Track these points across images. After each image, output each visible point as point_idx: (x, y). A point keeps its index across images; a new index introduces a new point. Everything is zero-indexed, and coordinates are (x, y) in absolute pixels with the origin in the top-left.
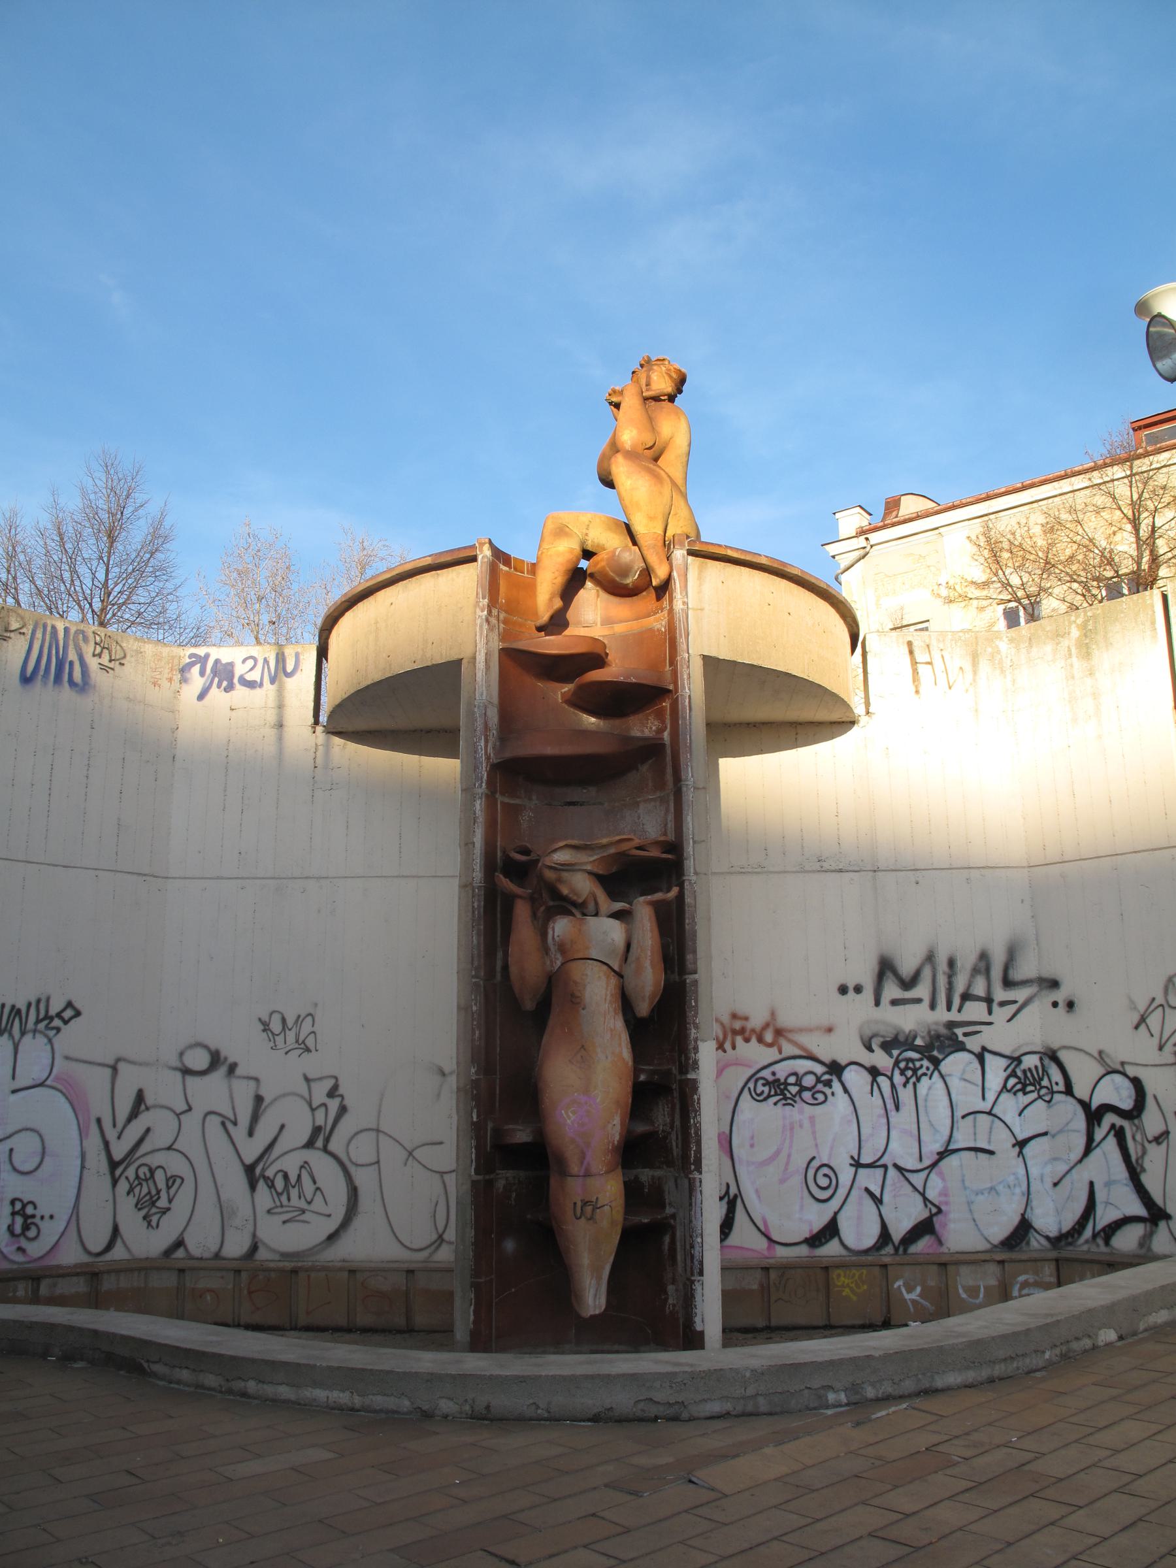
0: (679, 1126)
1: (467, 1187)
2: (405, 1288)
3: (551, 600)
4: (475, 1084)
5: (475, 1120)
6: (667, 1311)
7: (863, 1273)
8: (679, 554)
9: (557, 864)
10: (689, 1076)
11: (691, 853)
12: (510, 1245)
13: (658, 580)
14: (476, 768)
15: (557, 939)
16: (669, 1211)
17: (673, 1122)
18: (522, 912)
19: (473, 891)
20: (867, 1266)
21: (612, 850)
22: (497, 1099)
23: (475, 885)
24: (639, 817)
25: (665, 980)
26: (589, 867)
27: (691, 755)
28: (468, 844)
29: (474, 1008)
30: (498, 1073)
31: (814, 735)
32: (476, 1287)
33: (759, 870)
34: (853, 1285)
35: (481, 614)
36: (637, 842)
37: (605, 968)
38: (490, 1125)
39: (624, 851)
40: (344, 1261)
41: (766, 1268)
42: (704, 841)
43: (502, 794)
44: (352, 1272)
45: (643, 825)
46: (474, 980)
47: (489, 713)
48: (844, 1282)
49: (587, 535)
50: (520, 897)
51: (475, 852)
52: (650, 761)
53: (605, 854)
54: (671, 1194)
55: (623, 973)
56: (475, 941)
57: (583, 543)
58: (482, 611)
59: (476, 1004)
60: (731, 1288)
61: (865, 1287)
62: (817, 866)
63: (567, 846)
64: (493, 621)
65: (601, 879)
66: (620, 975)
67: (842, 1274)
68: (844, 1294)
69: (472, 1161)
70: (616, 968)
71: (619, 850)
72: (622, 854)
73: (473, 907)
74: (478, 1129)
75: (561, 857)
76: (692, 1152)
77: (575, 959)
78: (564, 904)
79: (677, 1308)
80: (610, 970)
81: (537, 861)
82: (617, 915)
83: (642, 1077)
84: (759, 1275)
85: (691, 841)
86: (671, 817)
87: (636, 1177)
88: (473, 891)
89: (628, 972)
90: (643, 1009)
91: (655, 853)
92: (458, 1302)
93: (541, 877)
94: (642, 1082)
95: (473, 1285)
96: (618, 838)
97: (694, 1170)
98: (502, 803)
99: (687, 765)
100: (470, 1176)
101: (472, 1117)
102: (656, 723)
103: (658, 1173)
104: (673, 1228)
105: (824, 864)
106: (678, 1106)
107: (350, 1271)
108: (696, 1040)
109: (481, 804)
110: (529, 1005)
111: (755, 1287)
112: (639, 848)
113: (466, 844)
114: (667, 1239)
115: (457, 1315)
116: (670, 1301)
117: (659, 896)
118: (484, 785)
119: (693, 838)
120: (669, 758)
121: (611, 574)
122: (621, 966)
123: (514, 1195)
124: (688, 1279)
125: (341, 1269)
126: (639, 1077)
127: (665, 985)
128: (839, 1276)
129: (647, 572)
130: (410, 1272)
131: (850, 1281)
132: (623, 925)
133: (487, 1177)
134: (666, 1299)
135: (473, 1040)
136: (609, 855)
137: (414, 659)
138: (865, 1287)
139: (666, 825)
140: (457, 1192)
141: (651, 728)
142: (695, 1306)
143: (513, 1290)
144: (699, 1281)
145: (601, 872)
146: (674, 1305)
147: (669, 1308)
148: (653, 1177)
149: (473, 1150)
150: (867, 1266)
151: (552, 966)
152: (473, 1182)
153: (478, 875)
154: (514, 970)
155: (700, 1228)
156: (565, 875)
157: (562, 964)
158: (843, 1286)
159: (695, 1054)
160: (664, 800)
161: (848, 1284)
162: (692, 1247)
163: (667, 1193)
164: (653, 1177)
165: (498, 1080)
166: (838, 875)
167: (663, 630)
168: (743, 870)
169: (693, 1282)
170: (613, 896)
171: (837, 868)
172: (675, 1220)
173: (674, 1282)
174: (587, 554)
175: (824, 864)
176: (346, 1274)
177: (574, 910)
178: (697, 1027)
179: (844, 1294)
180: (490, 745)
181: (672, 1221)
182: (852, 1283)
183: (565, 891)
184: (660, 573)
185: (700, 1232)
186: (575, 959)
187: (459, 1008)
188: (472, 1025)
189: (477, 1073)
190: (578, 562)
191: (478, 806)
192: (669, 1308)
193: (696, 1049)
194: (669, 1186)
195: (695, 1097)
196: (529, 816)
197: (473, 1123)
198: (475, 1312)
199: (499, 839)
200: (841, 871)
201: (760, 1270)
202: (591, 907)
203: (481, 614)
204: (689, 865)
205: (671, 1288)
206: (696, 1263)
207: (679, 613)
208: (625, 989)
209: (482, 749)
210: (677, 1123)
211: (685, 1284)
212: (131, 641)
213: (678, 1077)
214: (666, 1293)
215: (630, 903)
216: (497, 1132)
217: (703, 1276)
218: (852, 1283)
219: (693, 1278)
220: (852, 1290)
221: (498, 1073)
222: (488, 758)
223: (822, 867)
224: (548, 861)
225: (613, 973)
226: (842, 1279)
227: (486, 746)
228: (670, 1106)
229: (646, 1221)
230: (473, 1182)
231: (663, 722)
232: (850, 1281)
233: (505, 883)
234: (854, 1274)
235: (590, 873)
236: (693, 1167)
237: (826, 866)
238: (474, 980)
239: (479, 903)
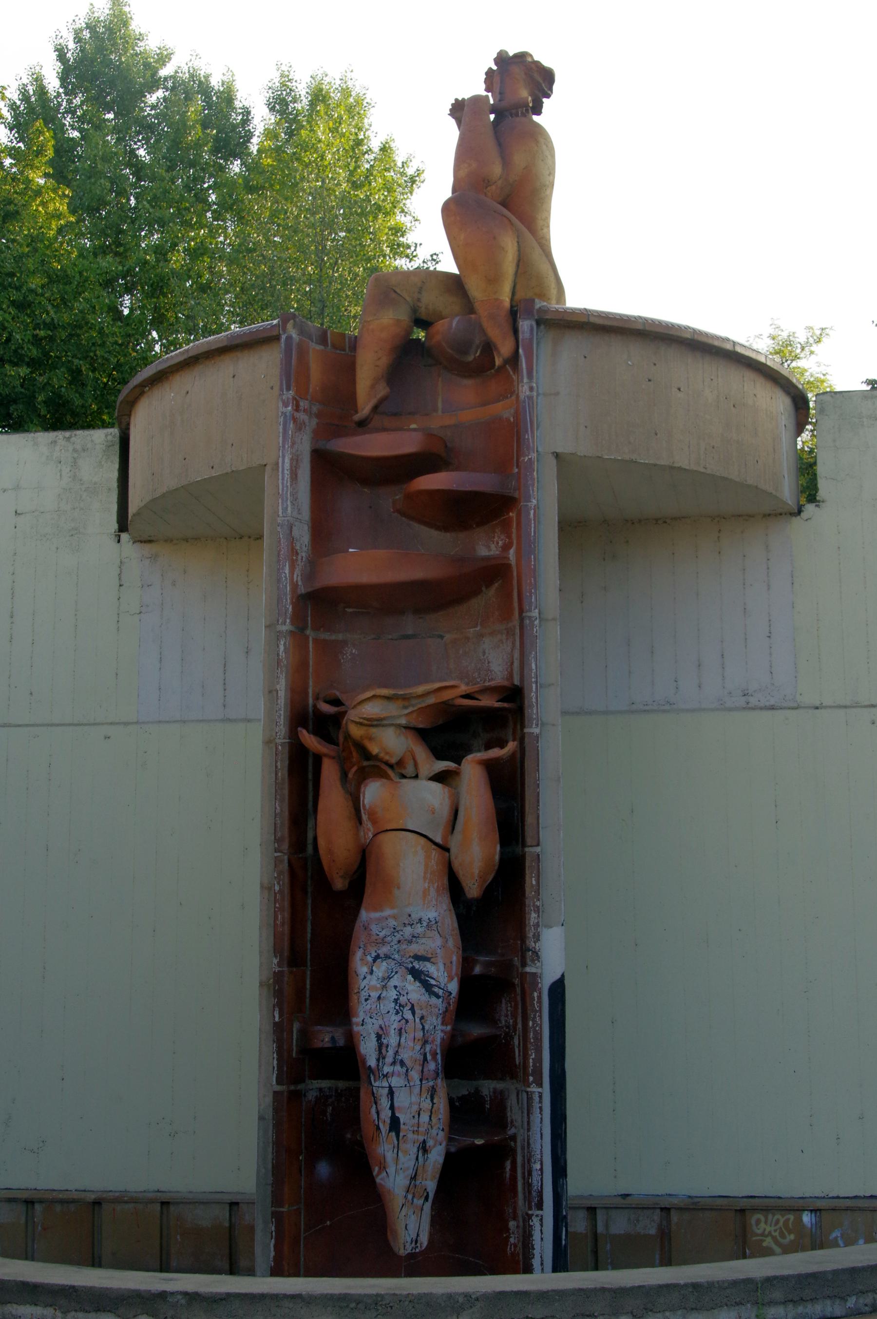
0: (521, 1030)
1: (269, 1099)
2: (227, 1224)
3: (373, 387)
4: (278, 977)
5: (277, 1019)
6: (509, 1252)
7: (788, 1220)
8: (525, 325)
9: (364, 719)
10: (528, 969)
11: (534, 700)
12: (323, 1169)
13: (501, 359)
14: (279, 600)
15: (367, 807)
16: (511, 1131)
17: (515, 1023)
18: (330, 772)
19: (277, 748)
20: (794, 1210)
21: (431, 700)
22: (308, 994)
23: (278, 741)
24: (484, 653)
25: (502, 853)
26: (403, 721)
27: (535, 580)
28: (271, 692)
29: (277, 888)
30: (309, 964)
31: (742, 532)
32: (277, 1217)
33: (667, 707)
34: (777, 1234)
35: (284, 410)
36: (464, 688)
37: (422, 840)
38: (296, 1026)
39: (446, 701)
40: (158, 1191)
41: (665, 1208)
42: (553, 684)
43: (316, 628)
44: (165, 1204)
45: (489, 662)
46: (276, 854)
47: (296, 532)
48: (765, 1230)
49: (419, 300)
50: (326, 755)
51: (279, 701)
52: (496, 585)
53: (423, 705)
54: (514, 1113)
55: (449, 847)
56: (278, 808)
57: (415, 310)
58: (286, 407)
59: (279, 883)
60: (622, 1232)
61: (792, 1237)
62: (741, 702)
63: (374, 696)
64: (302, 416)
65: (423, 734)
66: (444, 848)
67: (763, 1219)
68: (764, 1244)
69: (274, 1068)
70: (439, 840)
71: (439, 700)
72: (446, 704)
73: (276, 767)
74: (279, 1031)
75: (372, 709)
76: (531, 1061)
77: (387, 830)
78: (378, 764)
79: (518, 1249)
80: (430, 843)
81: (346, 712)
82: (440, 778)
83: (478, 970)
84: (657, 1216)
85: (534, 686)
86: (517, 655)
87: (477, 1091)
88: (277, 748)
89: (454, 844)
90: (473, 889)
91: (488, 702)
92: (259, 1235)
93: (348, 736)
94: (476, 975)
95: (274, 1214)
96: (437, 685)
97: (533, 1082)
98: (315, 641)
99: (531, 593)
100: (272, 1086)
101: (274, 1017)
102: (503, 537)
103: (500, 1085)
104: (513, 1152)
105: (751, 699)
106: (520, 1007)
107: (163, 1203)
108: (537, 925)
109: (285, 644)
110: (339, 884)
111: (653, 1232)
112: (467, 696)
113: (270, 692)
114: (508, 1165)
115: (258, 1250)
116: (512, 1240)
117: (495, 753)
118: (288, 621)
119: (536, 682)
120: (515, 582)
121: (449, 351)
122: (445, 838)
123: (330, 1109)
124: (527, 1214)
125: (152, 1201)
126: (472, 969)
127: (501, 860)
128: (758, 1222)
129: (488, 348)
130: (233, 1205)
131: (773, 1228)
132: (447, 789)
133: (292, 1088)
134: (508, 1237)
135: (275, 925)
136: (426, 707)
137: (211, 465)
138: (792, 1237)
139: (512, 663)
140: (259, 1105)
141: (498, 543)
142: (533, 1245)
143: (328, 1223)
144: (537, 1216)
145: (421, 726)
146: (515, 1246)
147: (511, 1248)
148: (495, 1090)
149: (275, 1055)
150: (794, 1210)
151: (365, 839)
152: (275, 1093)
153: (282, 730)
154: (321, 843)
155: (538, 1152)
156: (373, 730)
157: (375, 835)
158: (763, 1235)
159: (535, 942)
160: (510, 632)
161: (770, 1233)
162: (530, 1173)
163: (509, 1109)
164: (495, 1090)
165: (309, 973)
166: (770, 712)
167: (512, 420)
168: (646, 708)
169: (530, 1217)
170: (439, 754)
171: (767, 704)
172: (515, 1142)
173: (515, 1218)
174: (422, 323)
175: (751, 699)
176: (158, 1207)
177: (390, 772)
178: (537, 910)
179: (764, 1244)
180: (297, 572)
181: (512, 1144)
182: (775, 1231)
183: (374, 749)
184: (505, 348)
185: (539, 1157)
186: (387, 830)
187: (262, 887)
188: (275, 907)
189: (279, 965)
190: (409, 332)
191: (282, 648)
192: (511, 1248)
193: (537, 938)
194: (512, 1101)
195: (536, 994)
196: (352, 654)
197: (275, 1024)
198: (275, 1246)
199: (311, 684)
200: (772, 708)
201: (658, 1211)
202: (410, 770)
203: (284, 410)
204: (531, 712)
205: (512, 1224)
206: (534, 1194)
207: (524, 401)
208: (456, 865)
209: (286, 579)
210: (520, 1026)
211: (524, 1221)
212: (74, 101)
213: (520, 970)
214: (508, 1230)
215: (459, 764)
216: (304, 1034)
217: (542, 1210)
218: (775, 1231)
219: (530, 1212)
220: (774, 1239)
221: (309, 964)
222: (294, 586)
223: (748, 703)
224: (353, 715)
225: (434, 847)
226: (762, 1225)
227: (292, 572)
228: (513, 1003)
229: (479, 1142)
230: (275, 1093)
231: (509, 536)
232: (773, 1228)
233: (310, 740)
234: (777, 1222)
235: (406, 728)
236: (531, 1079)
237: (753, 701)
238: (276, 854)
239: (283, 765)
